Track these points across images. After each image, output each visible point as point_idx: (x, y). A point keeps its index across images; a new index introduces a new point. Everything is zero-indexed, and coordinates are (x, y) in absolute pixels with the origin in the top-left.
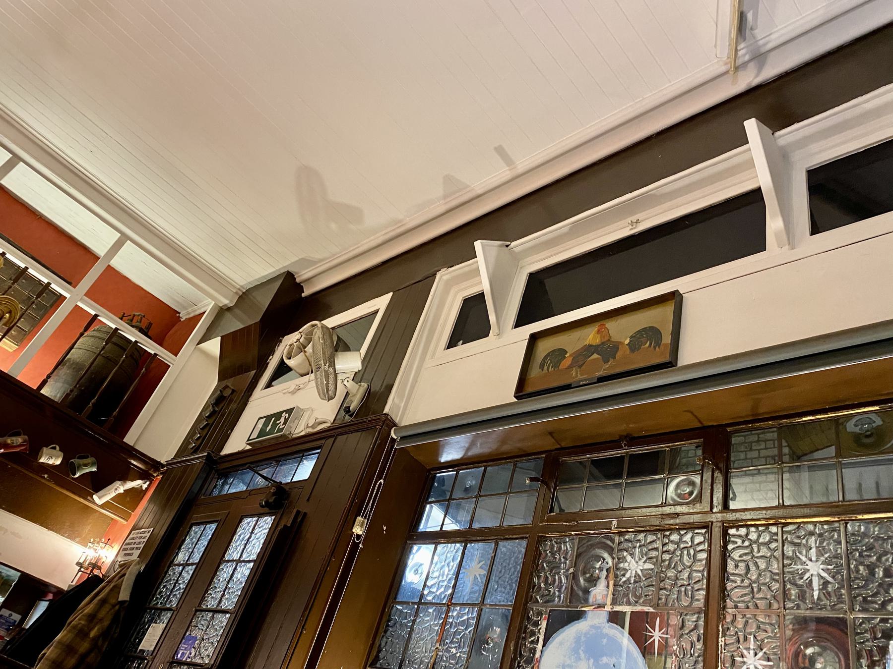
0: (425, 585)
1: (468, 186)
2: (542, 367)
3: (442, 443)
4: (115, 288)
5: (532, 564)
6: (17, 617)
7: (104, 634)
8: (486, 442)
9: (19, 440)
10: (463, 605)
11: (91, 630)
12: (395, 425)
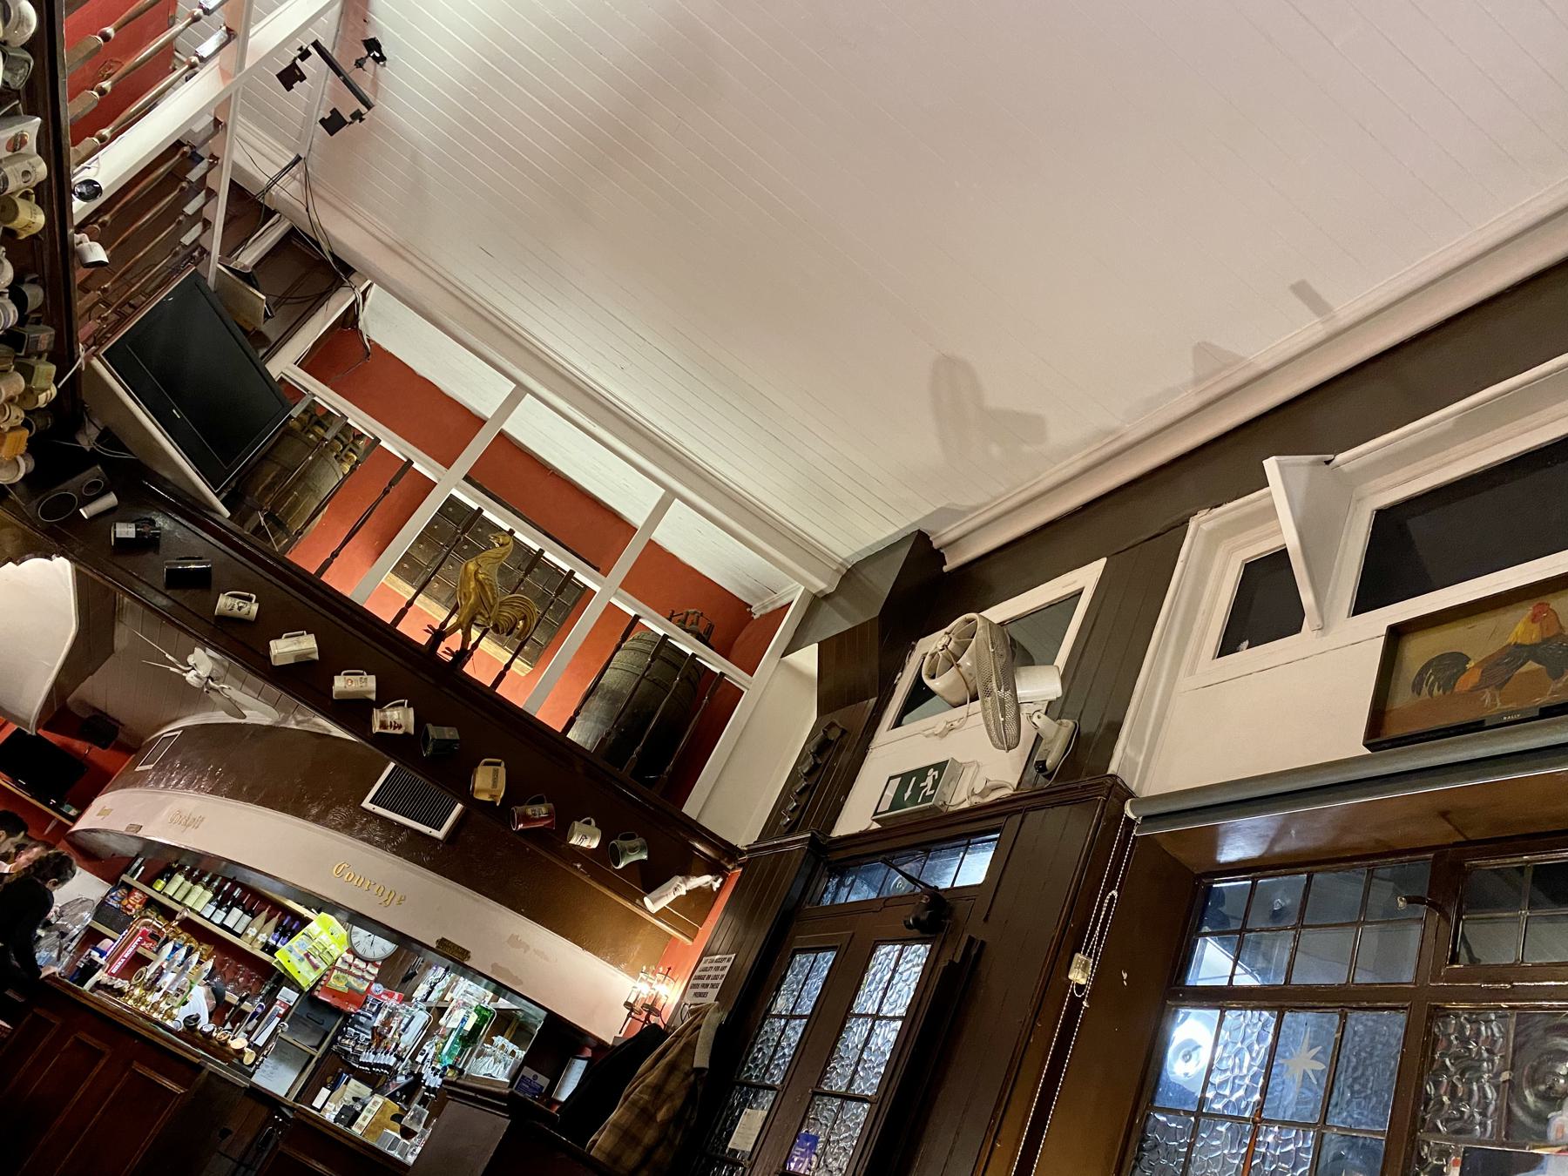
0: (1207, 1082)
1: (1242, 359)
2: (1417, 687)
3: (1221, 829)
4: (662, 575)
5: (1419, 1057)
6: (543, 1081)
7: (677, 1118)
8: (1310, 828)
9: (542, 810)
10: (1286, 1124)
11: (659, 1109)
12: (1131, 795)
